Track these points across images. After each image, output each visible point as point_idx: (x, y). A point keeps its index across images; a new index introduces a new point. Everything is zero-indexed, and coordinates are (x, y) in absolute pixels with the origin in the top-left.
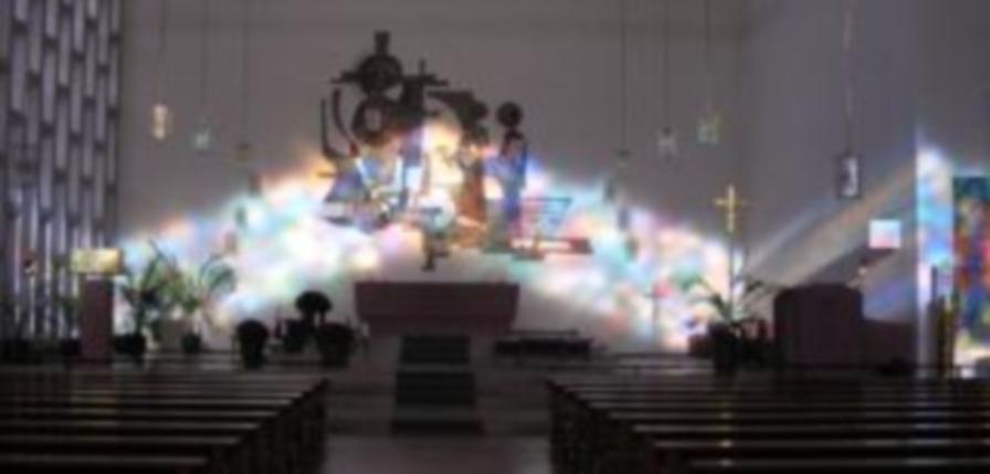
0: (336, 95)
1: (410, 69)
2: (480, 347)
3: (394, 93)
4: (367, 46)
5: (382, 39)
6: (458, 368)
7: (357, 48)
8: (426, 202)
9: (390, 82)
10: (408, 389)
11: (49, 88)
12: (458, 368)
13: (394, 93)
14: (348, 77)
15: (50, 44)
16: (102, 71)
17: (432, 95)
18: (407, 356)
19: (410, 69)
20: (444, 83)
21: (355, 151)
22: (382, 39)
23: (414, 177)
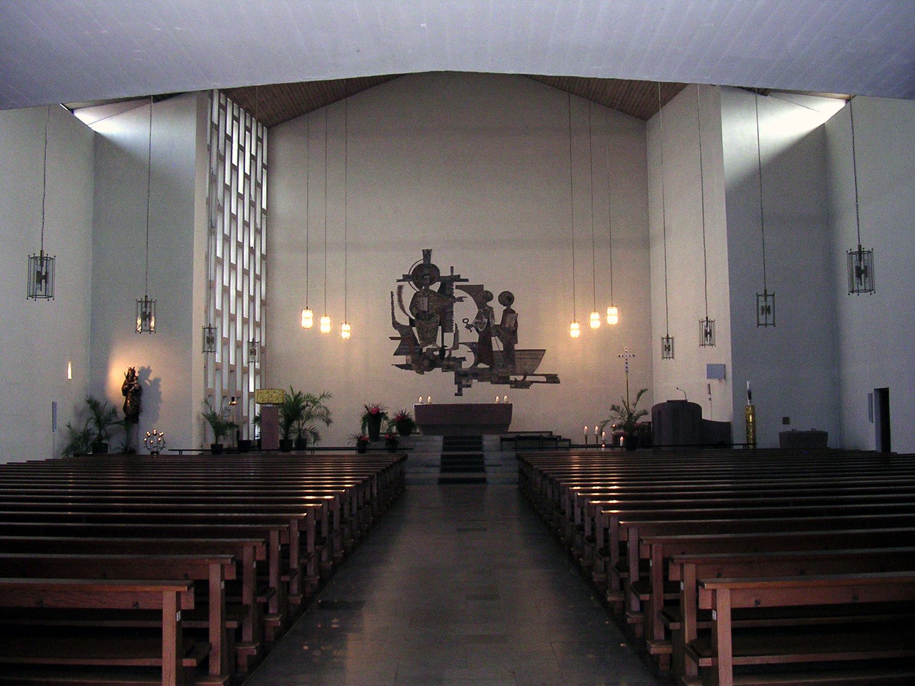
0: (400, 288)
1: (445, 272)
2: (490, 440)
3: (436, 287)
4: (419, 258)
5: (427, 254)
6: (481, 453)
7: (429, 248)
8: (455, 354)
9: (432, 282)
10: (447, 464)
11: (233, 293)
12: (481, 453)
13: (436, 287)
14: (406, 278)
15: (233, 267)
16: (258, 231)
17: (458, 287)
18: (448, 445)
19: (445, 272)
20: (467, 280)
21: (219, 416)
22: (427, 254)
23: (449, 338)
